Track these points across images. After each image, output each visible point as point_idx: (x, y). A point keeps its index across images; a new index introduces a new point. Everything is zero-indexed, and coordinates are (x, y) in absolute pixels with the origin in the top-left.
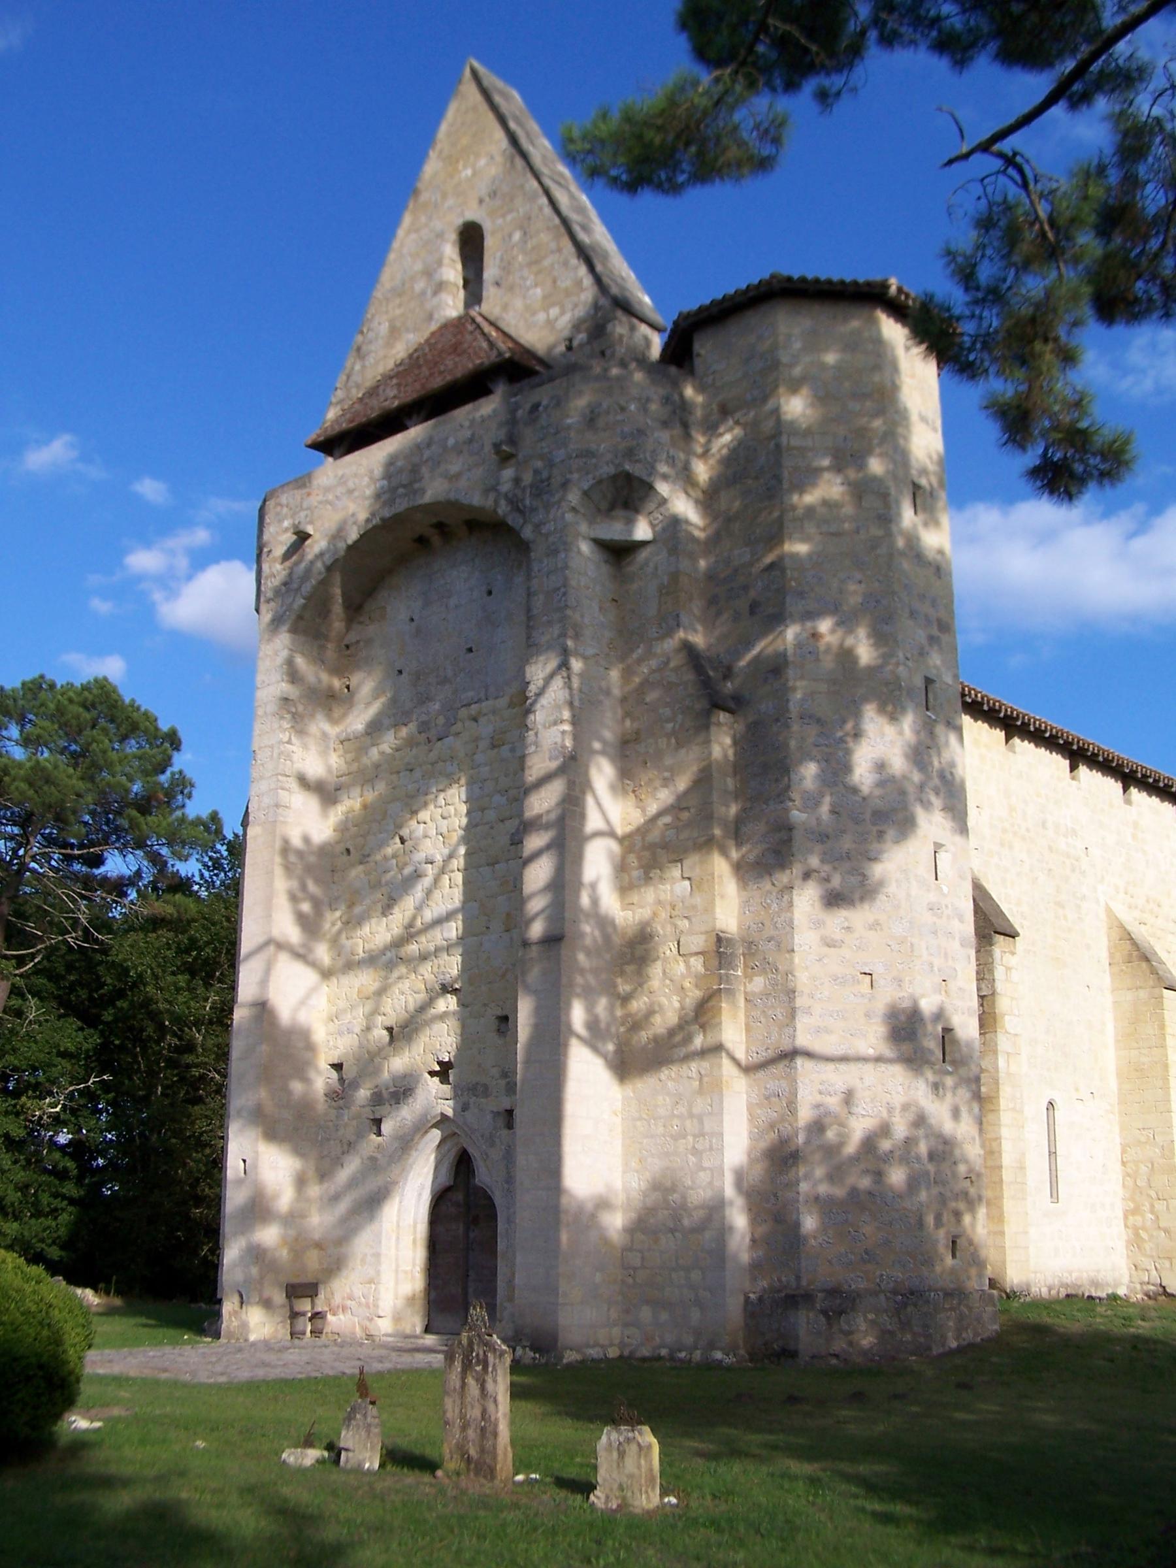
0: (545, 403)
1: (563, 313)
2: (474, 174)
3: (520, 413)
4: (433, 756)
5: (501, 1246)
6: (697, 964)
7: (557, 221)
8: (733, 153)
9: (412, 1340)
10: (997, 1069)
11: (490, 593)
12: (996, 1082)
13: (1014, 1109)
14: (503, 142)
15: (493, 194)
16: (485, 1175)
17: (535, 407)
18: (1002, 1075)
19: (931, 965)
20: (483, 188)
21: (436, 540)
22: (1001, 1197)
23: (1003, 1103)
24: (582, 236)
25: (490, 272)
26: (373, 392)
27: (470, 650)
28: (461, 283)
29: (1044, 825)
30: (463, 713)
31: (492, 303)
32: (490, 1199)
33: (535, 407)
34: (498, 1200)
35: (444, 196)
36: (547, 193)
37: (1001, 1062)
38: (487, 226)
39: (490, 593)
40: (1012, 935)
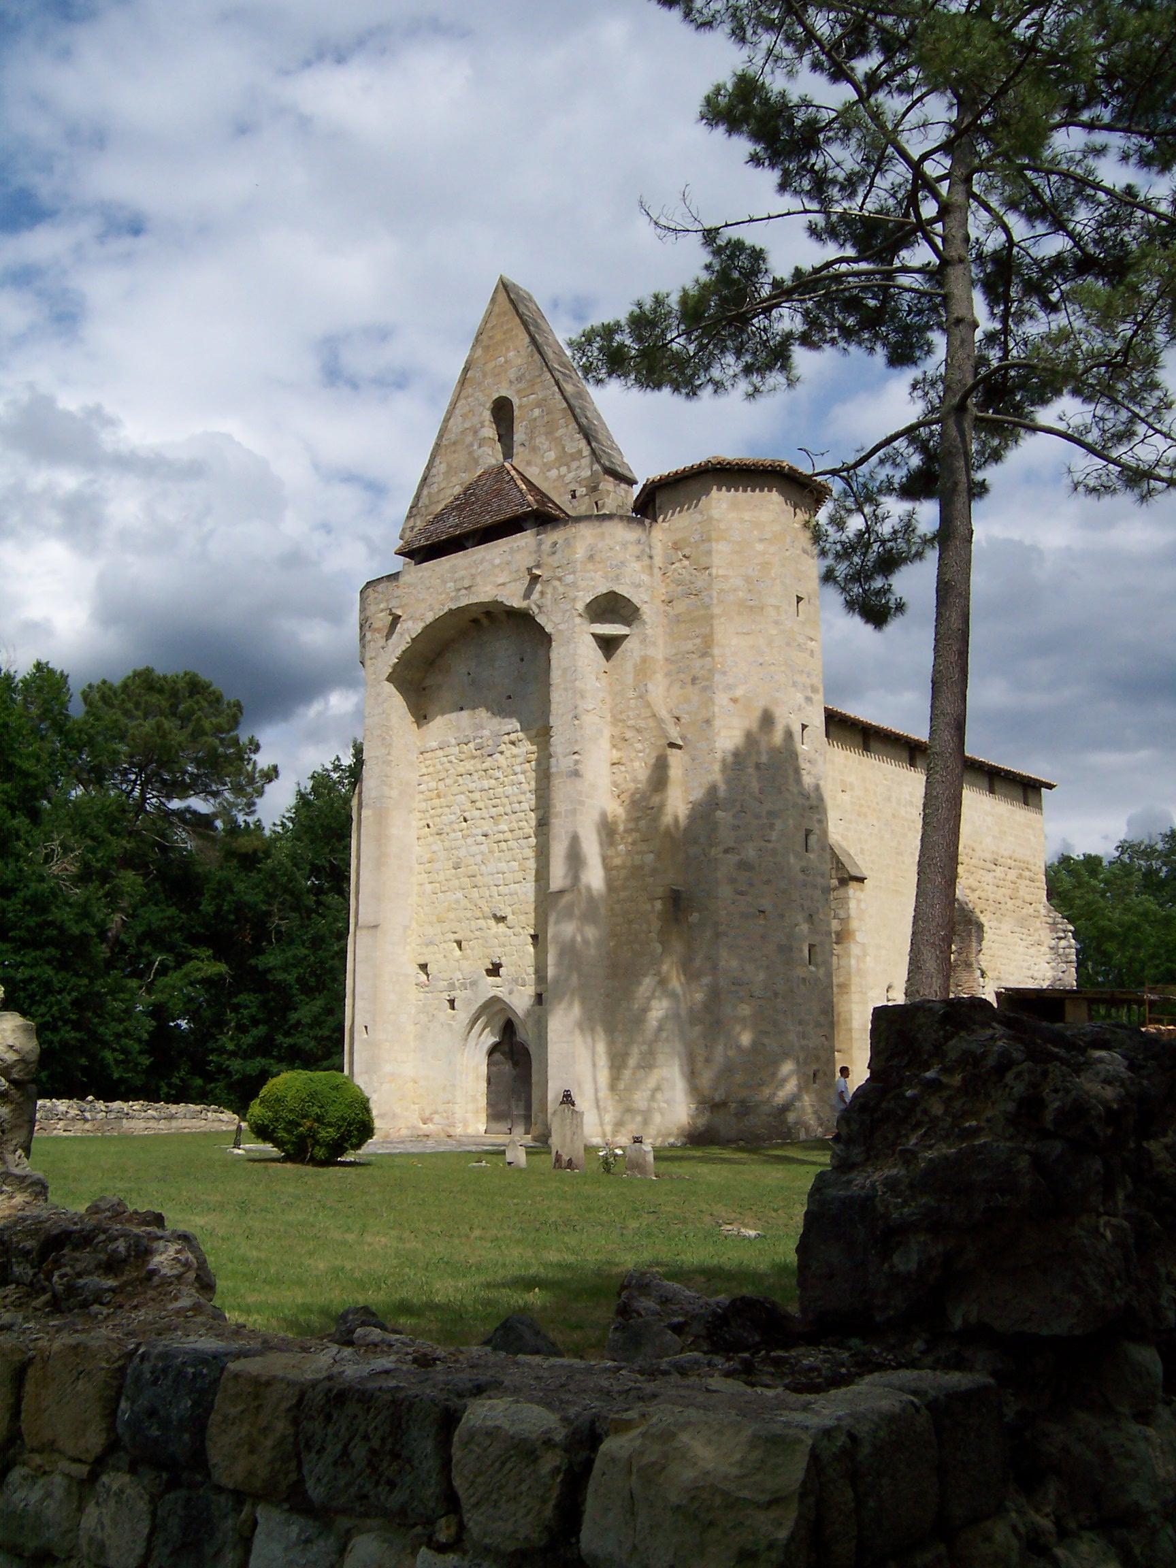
0: (560, 541)
1: (569, 472)
2: (506, 362)
3: (543, 547)
4: (485, 766)
5: (535, 1078)
6: (658, 905)
7: (565, 405)
8: (657, 994)
9: (601, 1095)
10: (850, 966)
11: (522, 660)
12: (849, 974)
13: (861, 992)
14: (527, 339)
15: (519, 379)
16: (526, 1034)
17: (555, 544)
18: (853, 971)
19: (802, 906)
20: (512, 373)
21: (485, 622)
22: (850, 1048)
23: (853, 988)
24: (584, 421)
25: (519, 435)
26: (439, 517)
27: (510, 697)
28: (497, 438)
29: (889, 799)
30: (506, 738)
31: (520, 457)
32: (527, 1051)
33: (555, 544)
34: (533, 1050)
35: (485, 375)
36: (557, 383)
37: (853, 962)
38: (516, 402)
39: (522, 660)
40: (861, 880)
